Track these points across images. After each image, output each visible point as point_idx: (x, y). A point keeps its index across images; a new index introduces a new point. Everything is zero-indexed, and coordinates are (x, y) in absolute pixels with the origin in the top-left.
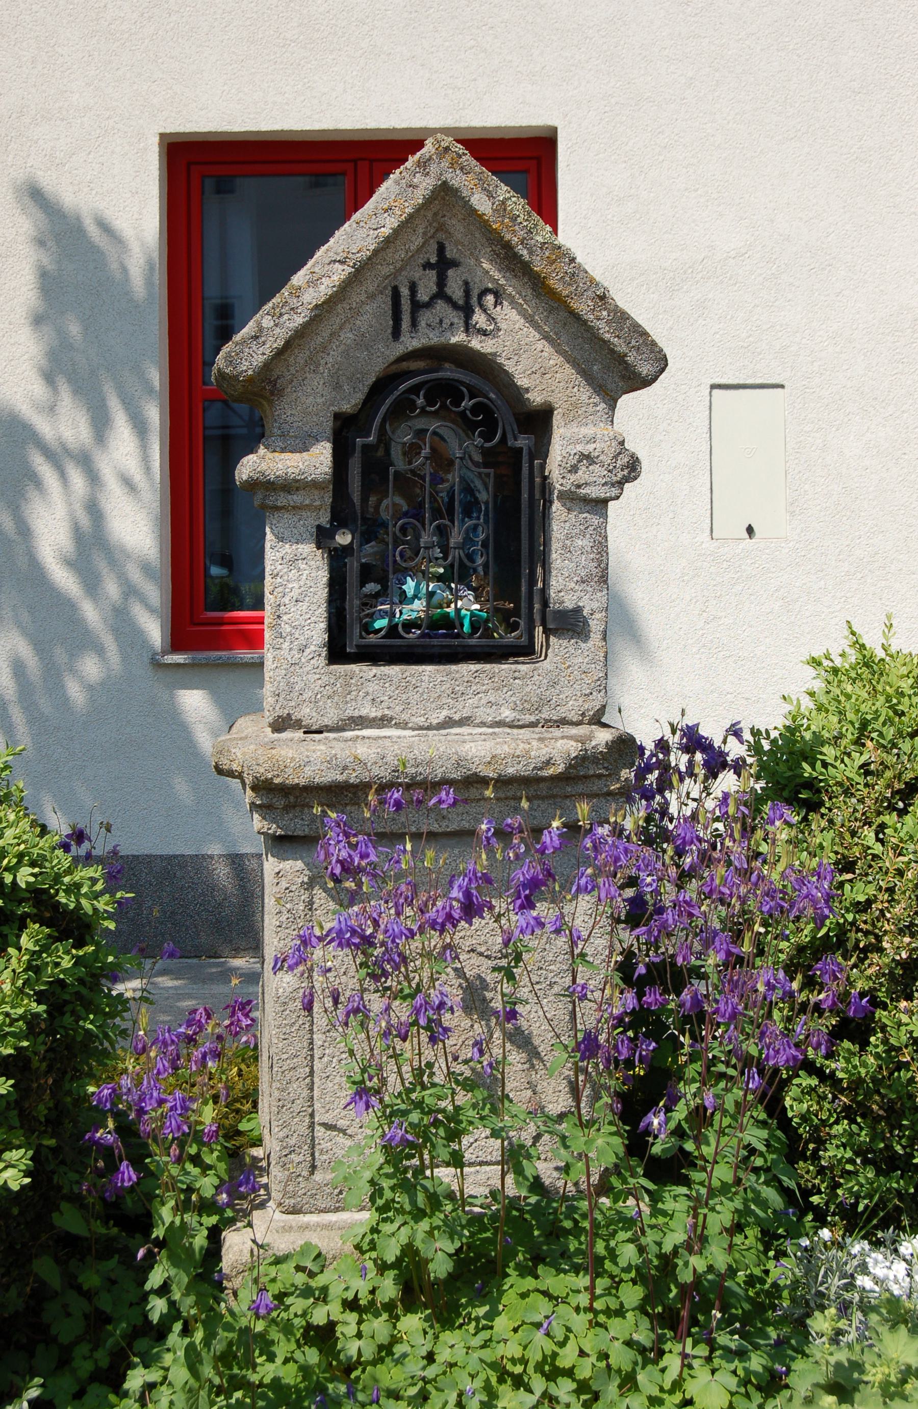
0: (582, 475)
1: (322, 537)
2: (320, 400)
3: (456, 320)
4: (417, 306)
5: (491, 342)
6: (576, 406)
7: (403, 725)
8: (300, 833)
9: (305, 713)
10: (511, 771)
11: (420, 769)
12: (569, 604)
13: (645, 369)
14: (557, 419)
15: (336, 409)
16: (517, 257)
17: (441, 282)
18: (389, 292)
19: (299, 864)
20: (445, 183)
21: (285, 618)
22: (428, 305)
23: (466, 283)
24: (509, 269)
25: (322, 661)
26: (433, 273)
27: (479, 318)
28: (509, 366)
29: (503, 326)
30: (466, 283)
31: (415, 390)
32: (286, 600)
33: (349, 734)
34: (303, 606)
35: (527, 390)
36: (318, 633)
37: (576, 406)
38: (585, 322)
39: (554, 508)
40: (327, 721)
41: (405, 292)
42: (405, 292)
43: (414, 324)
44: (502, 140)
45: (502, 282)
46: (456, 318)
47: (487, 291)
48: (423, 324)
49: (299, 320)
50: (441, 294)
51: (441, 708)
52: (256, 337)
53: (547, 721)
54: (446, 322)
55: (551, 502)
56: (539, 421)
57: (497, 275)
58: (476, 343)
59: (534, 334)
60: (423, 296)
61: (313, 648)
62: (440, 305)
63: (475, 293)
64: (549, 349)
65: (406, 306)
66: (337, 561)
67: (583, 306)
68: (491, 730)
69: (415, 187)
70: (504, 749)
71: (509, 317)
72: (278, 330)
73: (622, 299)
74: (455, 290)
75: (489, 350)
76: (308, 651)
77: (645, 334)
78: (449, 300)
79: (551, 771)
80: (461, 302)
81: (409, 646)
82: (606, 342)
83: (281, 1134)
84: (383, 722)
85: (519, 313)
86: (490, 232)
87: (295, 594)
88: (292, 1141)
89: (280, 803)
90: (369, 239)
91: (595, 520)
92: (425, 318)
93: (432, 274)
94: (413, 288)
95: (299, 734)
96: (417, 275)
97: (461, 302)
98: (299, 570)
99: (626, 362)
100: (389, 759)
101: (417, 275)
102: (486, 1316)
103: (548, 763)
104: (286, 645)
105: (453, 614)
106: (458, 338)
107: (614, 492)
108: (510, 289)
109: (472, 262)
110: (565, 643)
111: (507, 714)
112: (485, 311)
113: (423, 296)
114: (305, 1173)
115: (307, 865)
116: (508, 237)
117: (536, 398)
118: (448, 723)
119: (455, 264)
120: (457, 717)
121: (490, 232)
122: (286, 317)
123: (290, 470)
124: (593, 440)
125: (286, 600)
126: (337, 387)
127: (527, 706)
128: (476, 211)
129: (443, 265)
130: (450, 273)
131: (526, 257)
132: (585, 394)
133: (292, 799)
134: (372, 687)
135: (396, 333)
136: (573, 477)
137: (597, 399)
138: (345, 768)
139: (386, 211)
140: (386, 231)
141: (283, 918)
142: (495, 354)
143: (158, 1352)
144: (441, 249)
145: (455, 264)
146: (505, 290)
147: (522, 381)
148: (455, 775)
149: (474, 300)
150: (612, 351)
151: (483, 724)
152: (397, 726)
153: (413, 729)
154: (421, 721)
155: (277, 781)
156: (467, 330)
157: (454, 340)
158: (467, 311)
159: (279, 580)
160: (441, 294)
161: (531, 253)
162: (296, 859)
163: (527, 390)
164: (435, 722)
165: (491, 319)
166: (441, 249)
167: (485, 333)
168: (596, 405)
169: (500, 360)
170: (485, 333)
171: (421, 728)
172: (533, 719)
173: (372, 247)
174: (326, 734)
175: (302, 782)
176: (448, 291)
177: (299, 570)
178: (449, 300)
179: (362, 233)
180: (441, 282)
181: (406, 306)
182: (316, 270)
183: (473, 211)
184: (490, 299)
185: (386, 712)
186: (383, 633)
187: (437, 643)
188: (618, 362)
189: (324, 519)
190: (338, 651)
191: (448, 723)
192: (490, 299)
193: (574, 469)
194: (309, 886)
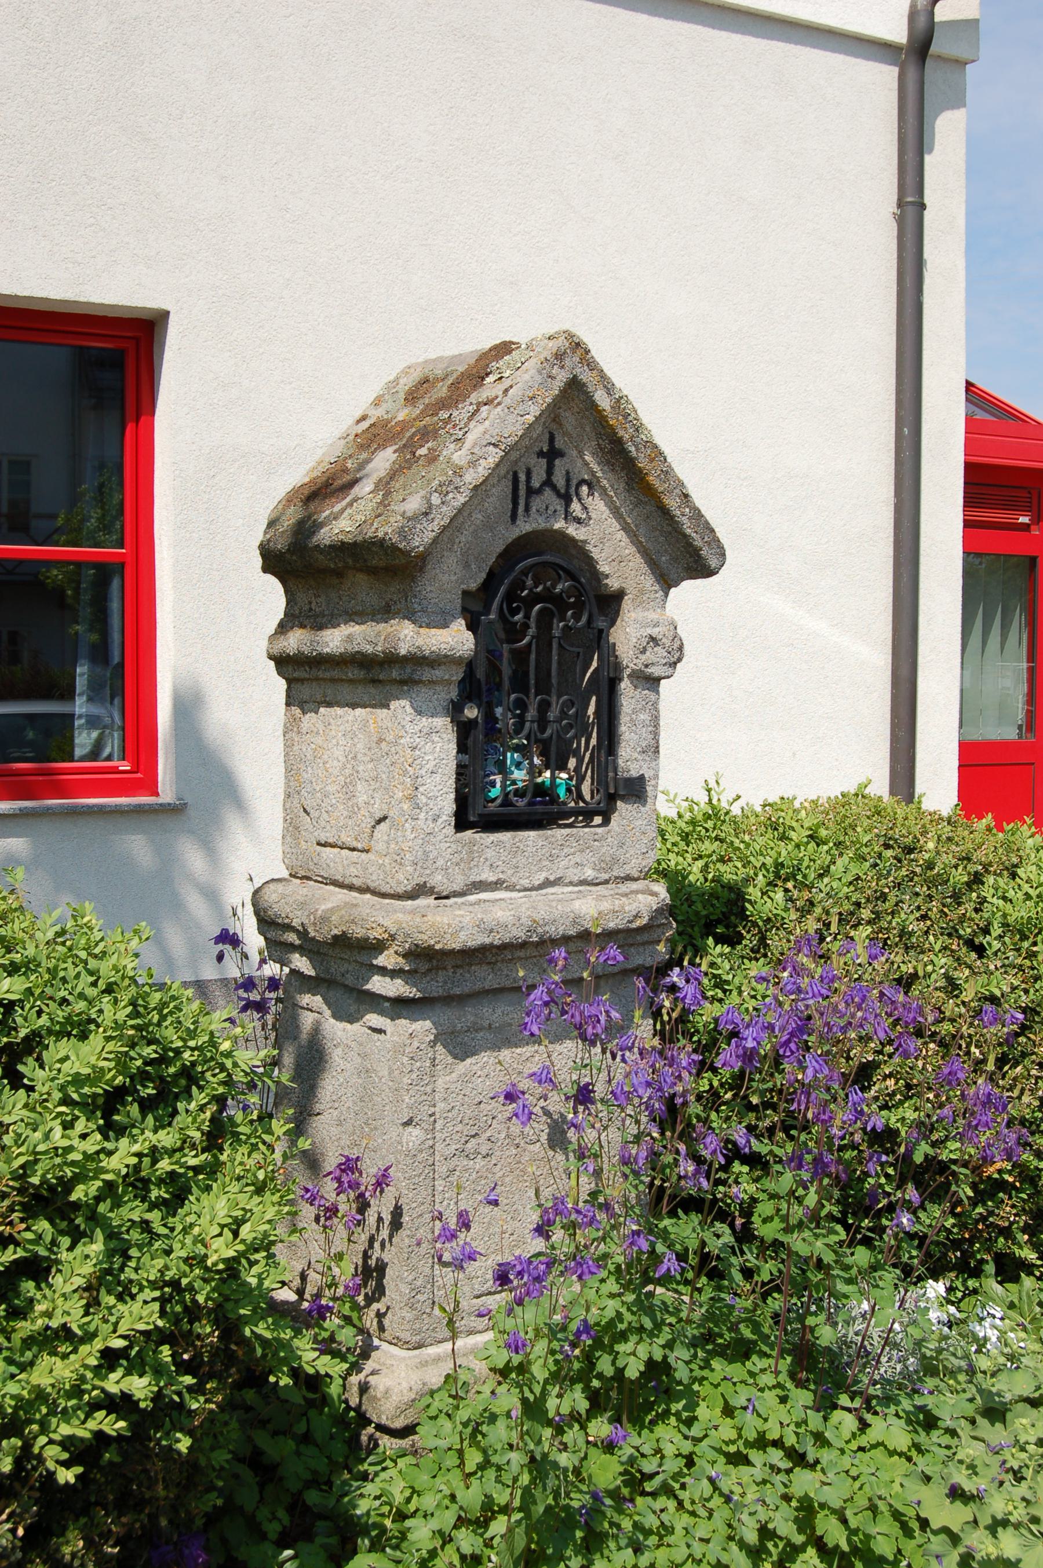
0: (649, 656)
1: (455, 710)
2: (453, 578)
3: (558, 508)
4: (531, 492)
5: (584, 530)
6: (642, 592)
7: (511, 888)
8: (435, 994)
9: (438, 880)
10: (611, 925)
11: (547, 928)
12: (634, 774)
13: (713, 563)
14: (627, 603)
15: (464, 587)
16: (623, 452)
17: (550, 471)
18: (510, 477)
19: (428, 1024)
20: (575, 376)
21: (421, 789)
22: (539, 491)
23: (568, 473)
24: (608, 462)
25: (451, 830)
26: (544, 462)
27: (575, 507)
28: (595, 553)
29: (593, 515)
30: (568, 473)
31: (525, 573)
32: (423, 772)
33: (472, 898)
34: (437, 778)
35: (607, 576)
36: (448, 805)
37: (642, 592)
38: (672, 517)
39: (623, 685)
40: (456, 887)
41: (522, 477)
42: (522, 477)
43: (527, 509)
44: (105, 318)
45: (599, 474)
46: (558, 504)
47: (583, 482)
48: (534, 509)
49: (462, 499)
50: (548, 483)
51: (541, 870)
52: (426, 514)
53: (616, 878)
54: (551, 508)
55: (621, 680)
56: (610, 603)
57: (595, 467)
58: (572, 530)
59: (616, 525)
60: (536, 484)
61: (445, 818)
62: (548, 492)
63: (574, 482)
64: (626, 540)
65: (522, 492)
66: (464, 731)
67: (672, 503)
68: (576, 889)
69: (553, 378)
70: (605, 906)
71: (598, 506)
72: (444, 509)
73: (699, 499)
74: (559, 480)
75: (582, 538)
76: (440, 820)
77: (713, 531)
78: (554, 488)
79: (638, 923)
80: (563, 491)
81: (519, 814)
82: (685, 535)
83: (411, 1278)
84: (496, 885)
85: (606, 505)
86: (604, 427)
87: (430, 766)
88: (419, 1283)
89: (424, 967)
90: (518, 425)
91: (653, 696)
92: (537, 503)
93: (544, 462)
94: (529, 473)
95: (430, 901)
96: (533, 462)
97: (563, 491)
98: (433, 742)
99: (699, 556)
100: (524, 920)
101: (533, 462)
102: (685, 1408)
103: (637, 916)
104: (422, 816)
105: (548, 783)
106: (559, 525)
107: (667, 671)
108: (605, 482)
109: (575, 453)
110: (630, 807)
111: (589, 873)
112: (580, 500)
113: (536, 484)
114: (428, 1310)
115: (434, 1024)
116: (621, 433)
117: (613, 584)
118: (547, 884)
119: (561, 454)
120: (552, 878)
121: (604, 427)
122: (451, 495)
123: (443, 646)
124: (656, 625)
125: (423, 772)
126: (467, 565)
127: (603, 865)
128: (597, 406)
129: (552, 454)
130: (557, 462)
131: (634, 454)
132: (649, 582)
133: (435, 962)
134: (490, 853)
135: (514, 517)
136: (643, 657)
137: (657, 587)
138: (491, 931)
139: (531, 399)
140: (530, 418)
141: (414, 1076)
142: (585, 542)
143: (350, 1501)
144: (552, 439)
145: (561, 454)
146: (599, 482)
147: (604, 568)
148: (572, 932)
149: (572, 490)
150: (691, 545)
151: (571, 883)
152: (507, 889)
153: (519, 891)
154: (526, 883)
155: (437, 947)
156: (566, 519)
157: (557, 526)
158: (567, 500)
159: (417, 752)
160: (548, 483)
161: (637, 450)
162: (425, 1019)
163: (607, 576)
164: (537, 883)
165: (585, 508)
166: (552, 439)
167: (578, 521)
168: (656, 592)
169: (589, 547)
170: (578, 521)
171: (526, 890)
172: (606, 876)
173: (520, 433)
174: (452, 900)
175: (457, 946)
176: (554, 479)
177: (433, 742)
178: (554, 488)
179: (511, 418)
180: (550, 471)
181: (522, 492)
182: (475, 451)
183: (594, 406)
184: (585, 489)
185: (501, 876)
186: (499, 801)
187: (537, 811)
188: (684, 552)
189: (454, 694)
190: (462, 823)
191: (547, 884)
192: (585, 489)
193: (644, 651)
194: (433, 1044)
